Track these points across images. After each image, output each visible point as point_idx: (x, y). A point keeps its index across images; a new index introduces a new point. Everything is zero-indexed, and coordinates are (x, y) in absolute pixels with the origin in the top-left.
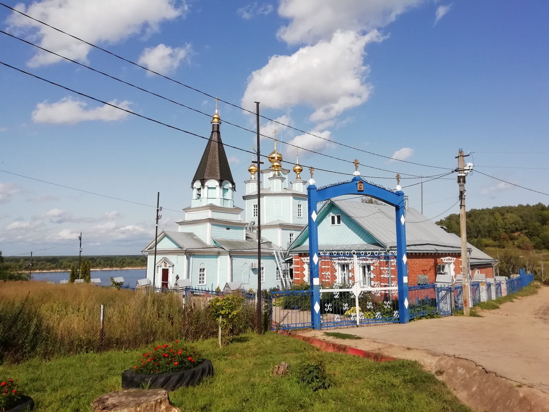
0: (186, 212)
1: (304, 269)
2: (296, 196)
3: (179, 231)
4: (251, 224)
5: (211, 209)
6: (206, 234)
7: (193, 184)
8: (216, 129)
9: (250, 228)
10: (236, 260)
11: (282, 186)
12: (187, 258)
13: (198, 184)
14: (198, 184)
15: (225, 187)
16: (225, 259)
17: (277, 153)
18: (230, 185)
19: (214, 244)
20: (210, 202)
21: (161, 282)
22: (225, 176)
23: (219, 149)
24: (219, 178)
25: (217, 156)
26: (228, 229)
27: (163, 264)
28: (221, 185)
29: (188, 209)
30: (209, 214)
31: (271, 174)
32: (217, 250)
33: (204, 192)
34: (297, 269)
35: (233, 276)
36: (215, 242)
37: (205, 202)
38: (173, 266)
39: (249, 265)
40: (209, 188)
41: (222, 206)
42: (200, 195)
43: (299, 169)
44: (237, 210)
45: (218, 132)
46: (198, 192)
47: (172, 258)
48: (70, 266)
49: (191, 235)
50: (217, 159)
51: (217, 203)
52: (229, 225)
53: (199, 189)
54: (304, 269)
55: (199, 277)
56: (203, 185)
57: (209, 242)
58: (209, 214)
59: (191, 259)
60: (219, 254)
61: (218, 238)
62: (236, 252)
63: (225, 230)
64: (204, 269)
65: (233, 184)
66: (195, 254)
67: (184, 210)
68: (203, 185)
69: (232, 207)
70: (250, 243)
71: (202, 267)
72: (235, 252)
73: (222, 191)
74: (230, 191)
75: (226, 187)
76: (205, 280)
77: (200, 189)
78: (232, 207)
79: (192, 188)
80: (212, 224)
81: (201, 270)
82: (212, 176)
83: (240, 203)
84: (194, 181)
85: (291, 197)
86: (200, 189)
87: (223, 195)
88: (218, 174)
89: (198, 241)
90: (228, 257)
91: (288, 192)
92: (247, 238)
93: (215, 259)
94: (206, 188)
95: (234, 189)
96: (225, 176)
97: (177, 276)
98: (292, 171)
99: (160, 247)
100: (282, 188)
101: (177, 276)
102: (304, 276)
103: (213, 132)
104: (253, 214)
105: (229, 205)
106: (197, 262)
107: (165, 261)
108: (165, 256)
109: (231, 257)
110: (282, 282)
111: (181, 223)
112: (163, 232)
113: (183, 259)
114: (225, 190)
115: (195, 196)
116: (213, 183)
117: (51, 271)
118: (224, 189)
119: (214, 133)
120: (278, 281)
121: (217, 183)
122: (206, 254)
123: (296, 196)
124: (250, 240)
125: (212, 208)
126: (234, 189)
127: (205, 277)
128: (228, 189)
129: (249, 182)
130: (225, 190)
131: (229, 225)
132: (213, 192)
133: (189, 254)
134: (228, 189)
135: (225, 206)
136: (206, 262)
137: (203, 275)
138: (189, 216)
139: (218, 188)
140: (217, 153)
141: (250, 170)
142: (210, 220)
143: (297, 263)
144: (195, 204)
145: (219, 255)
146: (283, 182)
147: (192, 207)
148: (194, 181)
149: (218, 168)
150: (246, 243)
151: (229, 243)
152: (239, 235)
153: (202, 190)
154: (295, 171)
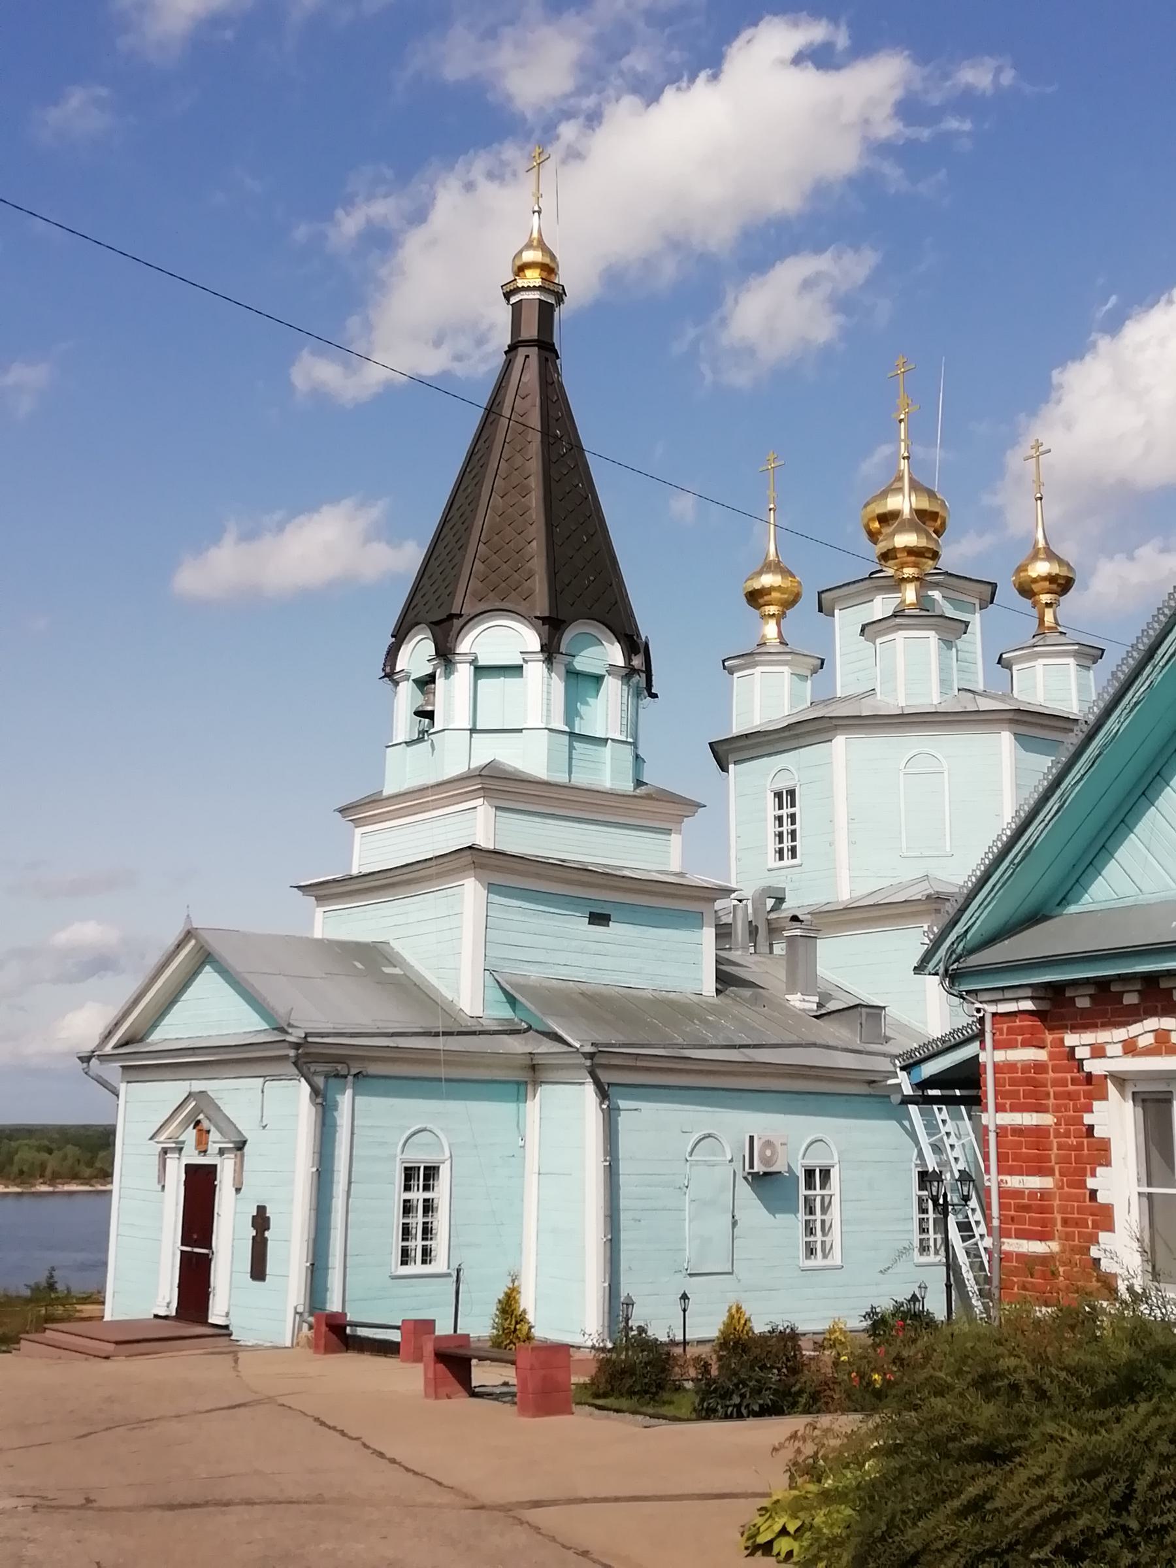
0: (358, 823)
1: (1101, 1153)
2: (1031, 724)
3: (318, 934)
4: (759, 900)
5: (486, 792)
6: (454, 948)
7: (392, 653)
8: (530, 331)
9: (753, 931)
10: (651, 1123)
11: (944, 669)
12: (316, 1092)
13: (417, 654)
14: (417, 654)
15: (580, 664)
16: (572, 1106)
17: (915, 486)
18: (614, 653)
19: (506, 1012)
20: (486, 751)
21: (179, 1247)
22: (582, 594)
23: (549, 440)
24: (542, 607)
25: (535, 484)
26: (599, 919)
27: (190, 1135)
28: (550, 651)
29: (361, 809)
30: (479, 824)
31: (881, 606)
32: (516, 1045)
33: (454, 693)
34: (1024, 1151)
35: (625, 1218)
36: (512, 1001)
37: (454, 756)
38: (241, 1146)
39: (730, 1149)
40: (481, 671)
41: (562, 778)
42: (430, 715)
43: (1052, 579)
44: (653, 805)
45: (546, 347)
46: (420, 701)
47: (236, 1097)
48: (43, 1166)
49: (370, 959)
50: (535, 500)
51: (532, 757)
52: (604, 898)
53: (426, 683)
54: (1101, 1153)
55: (397, 1220)
56: (445, 655)
57: (470, 997)
58: (479, 824)
59: (345, 1100)
60: (533, 1074)
61: (535, 974)
62: (636, 1064)
63: (580, 925)
64: (431, 1172)
65: (633, 644)
66: (373, 1069)
67: (343, 811)
68: (445, 655)
69: (628, 786)
70: (736, 1010)
71: (420, 1157)
72: (631, 1059)
73: (558, 685)
74: (613, 687)
75: (587, 661)
76: (440, 1245)
77: (431, 678)
78: (628, 786)
79: (390, 674)
80: (492, 888)
81: (409, 1173)
82: (501, 600)
83: (681, 767)
84: (400, 635)
85: (1006, 738)
86: (431, 678)
87: (571, 713)
88: (539, 585)
89: (412, 990)
90: (589, 1090)
91: (985, 704)
92: (725, 980)
93: (506, 1109)
94: (464, 672)
95: (640, 673)
96: (582, 594)
97: (261, 1209)
98: (1007, 593)
99: (176, 1030)
100: (944, 682)
101: (261, 1209)
102: (1104, 1218)
103: (512, 348)
104: (772, 845)
105: (607, 772)
106: (386, 1127)
107: (199, 1116)
108: (197, 1086)
109: (603, 1092)
110: (951, 1266)
111: (322, 892)
112: (189, 934)
113: (293, 1099)
114: (581, 683)
115: (404, 724)
116: (505, 638)
117: (60, 1188)
118: (573, 675)
119: (522, 351)
120: (932, 1258)
121: (531, 639)
122: (442, 1072)
123: (1031, 724)
124: (747, 993)
125: (497, 785)
126: (640, 673)
127: (441, 1221)
128: (598, 679)
129: (749, 658)
130: (581, 683)
131: (604, 898)
132: (506, 695)
133: (328, 1065)
134: (598, 679)
135: (581, 779)
136: (448, 1127)
137: (428, 1207)
138: (376, 848)
139: (536, 670)
140: (535, 466)
141: (755, 597)
142: (475, 859)
143: (1026, 1088)
144: (405, 770)
145: (537, 1083)
146: (948, 643)
147: (386, 793)
148: (400, 635)
149: (536, 548)
150: (713, 1009)
151: (593, 1004)
152: (676, 964)
153: (440, 681)
154: (1026, 590)
